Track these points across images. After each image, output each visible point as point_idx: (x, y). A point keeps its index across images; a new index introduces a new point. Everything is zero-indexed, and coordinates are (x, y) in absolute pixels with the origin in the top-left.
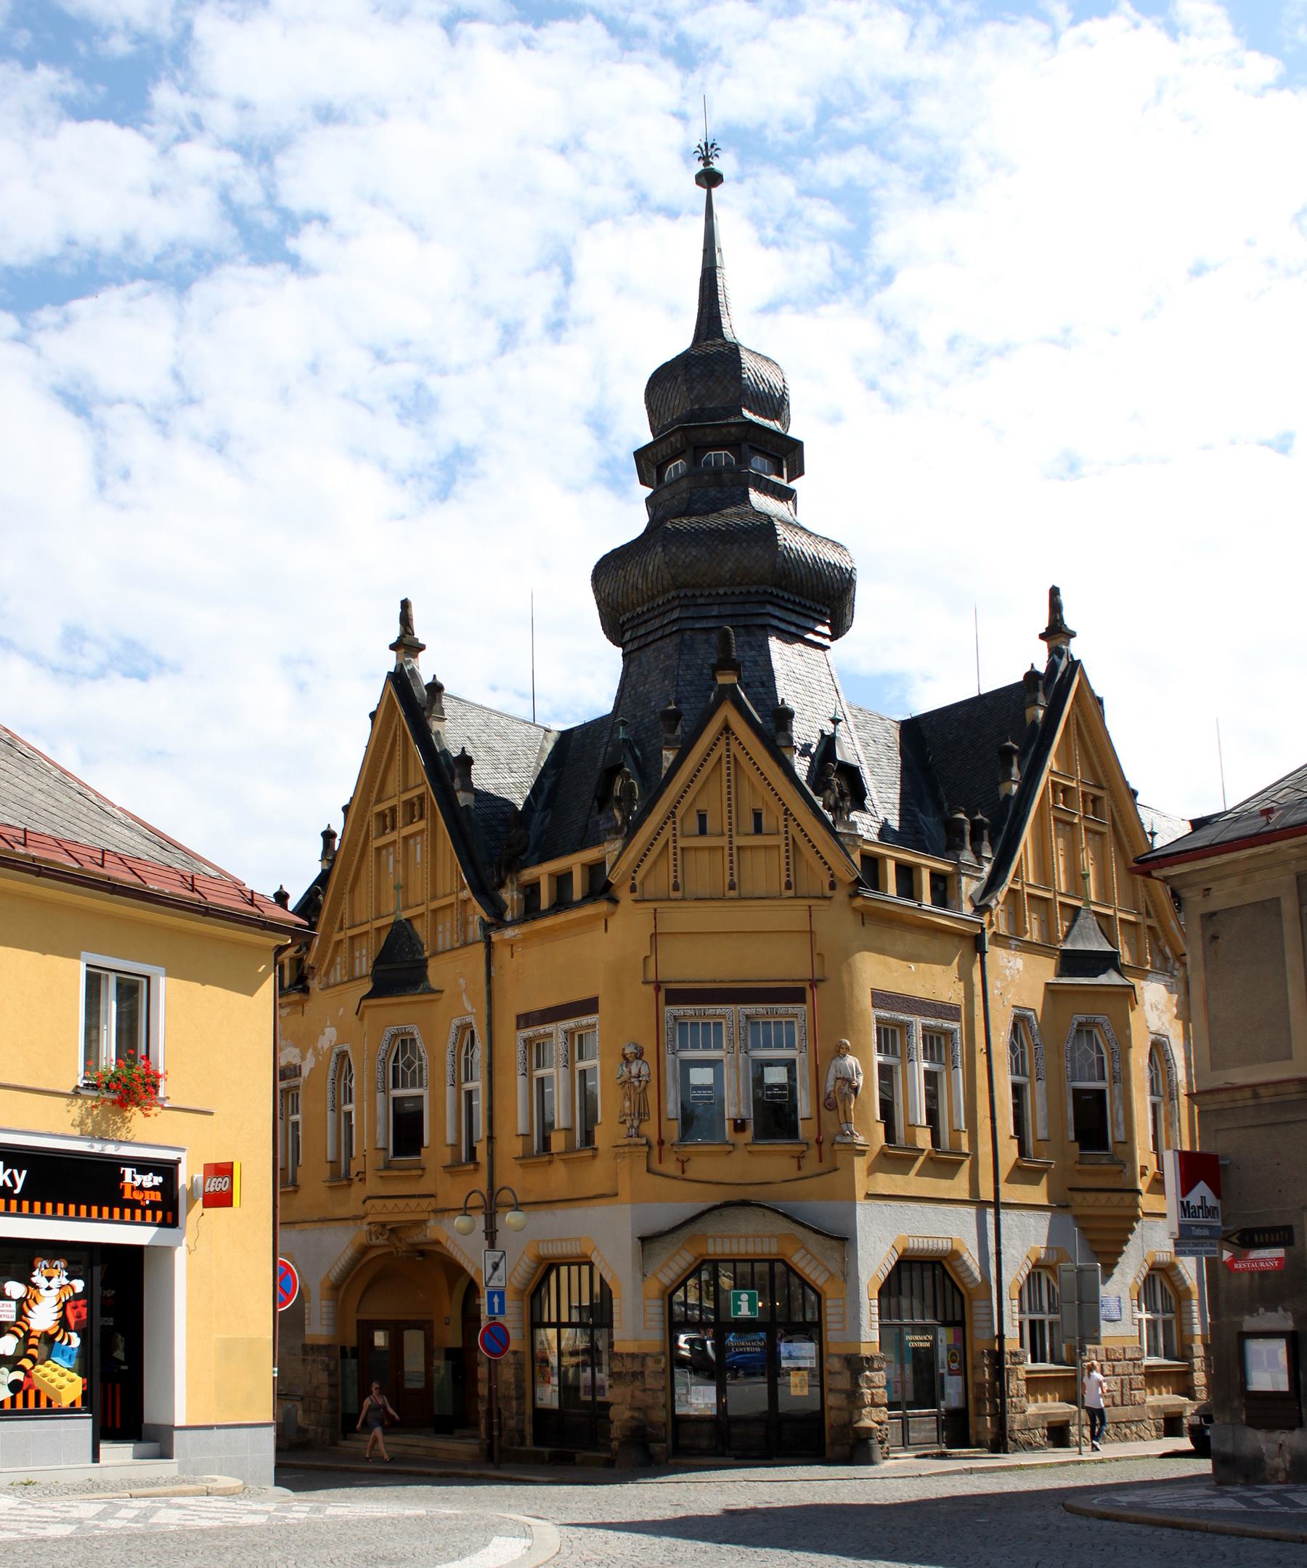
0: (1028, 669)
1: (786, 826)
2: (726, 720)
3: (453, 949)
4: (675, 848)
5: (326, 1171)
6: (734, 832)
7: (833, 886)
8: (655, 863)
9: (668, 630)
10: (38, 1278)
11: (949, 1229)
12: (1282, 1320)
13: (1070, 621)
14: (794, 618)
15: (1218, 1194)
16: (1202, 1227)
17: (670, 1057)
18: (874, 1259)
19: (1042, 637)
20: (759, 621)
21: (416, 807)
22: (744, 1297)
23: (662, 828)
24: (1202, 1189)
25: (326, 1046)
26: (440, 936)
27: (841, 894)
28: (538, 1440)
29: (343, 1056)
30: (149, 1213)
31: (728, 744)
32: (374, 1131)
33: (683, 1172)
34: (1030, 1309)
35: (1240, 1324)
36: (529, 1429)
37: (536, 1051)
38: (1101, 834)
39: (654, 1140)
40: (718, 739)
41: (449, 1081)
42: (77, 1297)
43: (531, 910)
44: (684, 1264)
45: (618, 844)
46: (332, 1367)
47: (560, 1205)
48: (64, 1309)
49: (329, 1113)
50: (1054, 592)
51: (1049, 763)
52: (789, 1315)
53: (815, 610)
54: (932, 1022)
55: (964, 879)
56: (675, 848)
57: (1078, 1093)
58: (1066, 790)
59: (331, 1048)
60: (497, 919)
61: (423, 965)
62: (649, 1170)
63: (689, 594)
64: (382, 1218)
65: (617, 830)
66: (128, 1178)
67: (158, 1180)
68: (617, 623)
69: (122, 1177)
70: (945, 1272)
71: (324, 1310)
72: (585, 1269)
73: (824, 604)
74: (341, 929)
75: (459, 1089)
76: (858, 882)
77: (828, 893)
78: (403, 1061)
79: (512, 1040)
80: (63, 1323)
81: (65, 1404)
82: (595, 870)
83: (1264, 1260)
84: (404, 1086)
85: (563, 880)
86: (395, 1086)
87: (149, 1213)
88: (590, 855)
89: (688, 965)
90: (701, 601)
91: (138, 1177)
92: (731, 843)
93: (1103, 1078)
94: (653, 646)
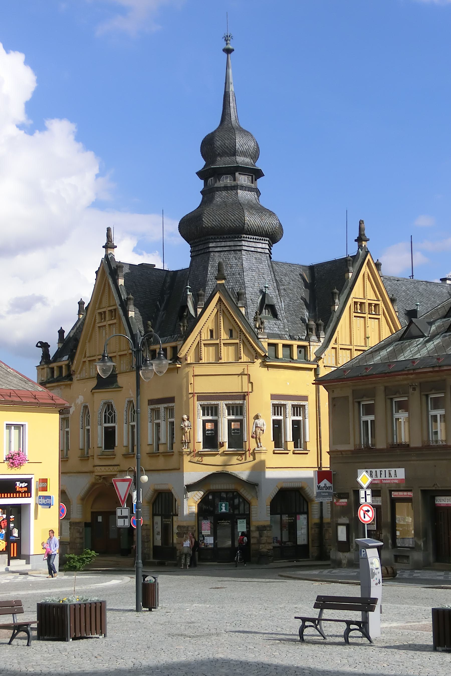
1: (240, 336)
5: (79, 453)
20: (238, 248)
21: (113, 313)
22: (224, 505)
25: (79, 403)
28: (154, 558)
29: (86, 407)
30: (23, 494)
32: (99, 439)
35: (337, 521)
36: (151, 553)
37: (156, 412)
41: (125, 421)
45: (182, 342)
46: (81, 531)
47: (161, 471)
52: (244, 512)
54: (296, 403)
59: (82, 404)
63: (213, 237)
64: (100, 474)
65: (182, 337)
66: (18, 485)
70: (301, 494)
74: (85, 357)
78: (109, 412)
79: (146, 410)
83: (343, 502)
84: (109, 422)
86: (105, 422)
87: (23, 494)
91: (21, 484)
92: (220, 342)
94: (201, 256)
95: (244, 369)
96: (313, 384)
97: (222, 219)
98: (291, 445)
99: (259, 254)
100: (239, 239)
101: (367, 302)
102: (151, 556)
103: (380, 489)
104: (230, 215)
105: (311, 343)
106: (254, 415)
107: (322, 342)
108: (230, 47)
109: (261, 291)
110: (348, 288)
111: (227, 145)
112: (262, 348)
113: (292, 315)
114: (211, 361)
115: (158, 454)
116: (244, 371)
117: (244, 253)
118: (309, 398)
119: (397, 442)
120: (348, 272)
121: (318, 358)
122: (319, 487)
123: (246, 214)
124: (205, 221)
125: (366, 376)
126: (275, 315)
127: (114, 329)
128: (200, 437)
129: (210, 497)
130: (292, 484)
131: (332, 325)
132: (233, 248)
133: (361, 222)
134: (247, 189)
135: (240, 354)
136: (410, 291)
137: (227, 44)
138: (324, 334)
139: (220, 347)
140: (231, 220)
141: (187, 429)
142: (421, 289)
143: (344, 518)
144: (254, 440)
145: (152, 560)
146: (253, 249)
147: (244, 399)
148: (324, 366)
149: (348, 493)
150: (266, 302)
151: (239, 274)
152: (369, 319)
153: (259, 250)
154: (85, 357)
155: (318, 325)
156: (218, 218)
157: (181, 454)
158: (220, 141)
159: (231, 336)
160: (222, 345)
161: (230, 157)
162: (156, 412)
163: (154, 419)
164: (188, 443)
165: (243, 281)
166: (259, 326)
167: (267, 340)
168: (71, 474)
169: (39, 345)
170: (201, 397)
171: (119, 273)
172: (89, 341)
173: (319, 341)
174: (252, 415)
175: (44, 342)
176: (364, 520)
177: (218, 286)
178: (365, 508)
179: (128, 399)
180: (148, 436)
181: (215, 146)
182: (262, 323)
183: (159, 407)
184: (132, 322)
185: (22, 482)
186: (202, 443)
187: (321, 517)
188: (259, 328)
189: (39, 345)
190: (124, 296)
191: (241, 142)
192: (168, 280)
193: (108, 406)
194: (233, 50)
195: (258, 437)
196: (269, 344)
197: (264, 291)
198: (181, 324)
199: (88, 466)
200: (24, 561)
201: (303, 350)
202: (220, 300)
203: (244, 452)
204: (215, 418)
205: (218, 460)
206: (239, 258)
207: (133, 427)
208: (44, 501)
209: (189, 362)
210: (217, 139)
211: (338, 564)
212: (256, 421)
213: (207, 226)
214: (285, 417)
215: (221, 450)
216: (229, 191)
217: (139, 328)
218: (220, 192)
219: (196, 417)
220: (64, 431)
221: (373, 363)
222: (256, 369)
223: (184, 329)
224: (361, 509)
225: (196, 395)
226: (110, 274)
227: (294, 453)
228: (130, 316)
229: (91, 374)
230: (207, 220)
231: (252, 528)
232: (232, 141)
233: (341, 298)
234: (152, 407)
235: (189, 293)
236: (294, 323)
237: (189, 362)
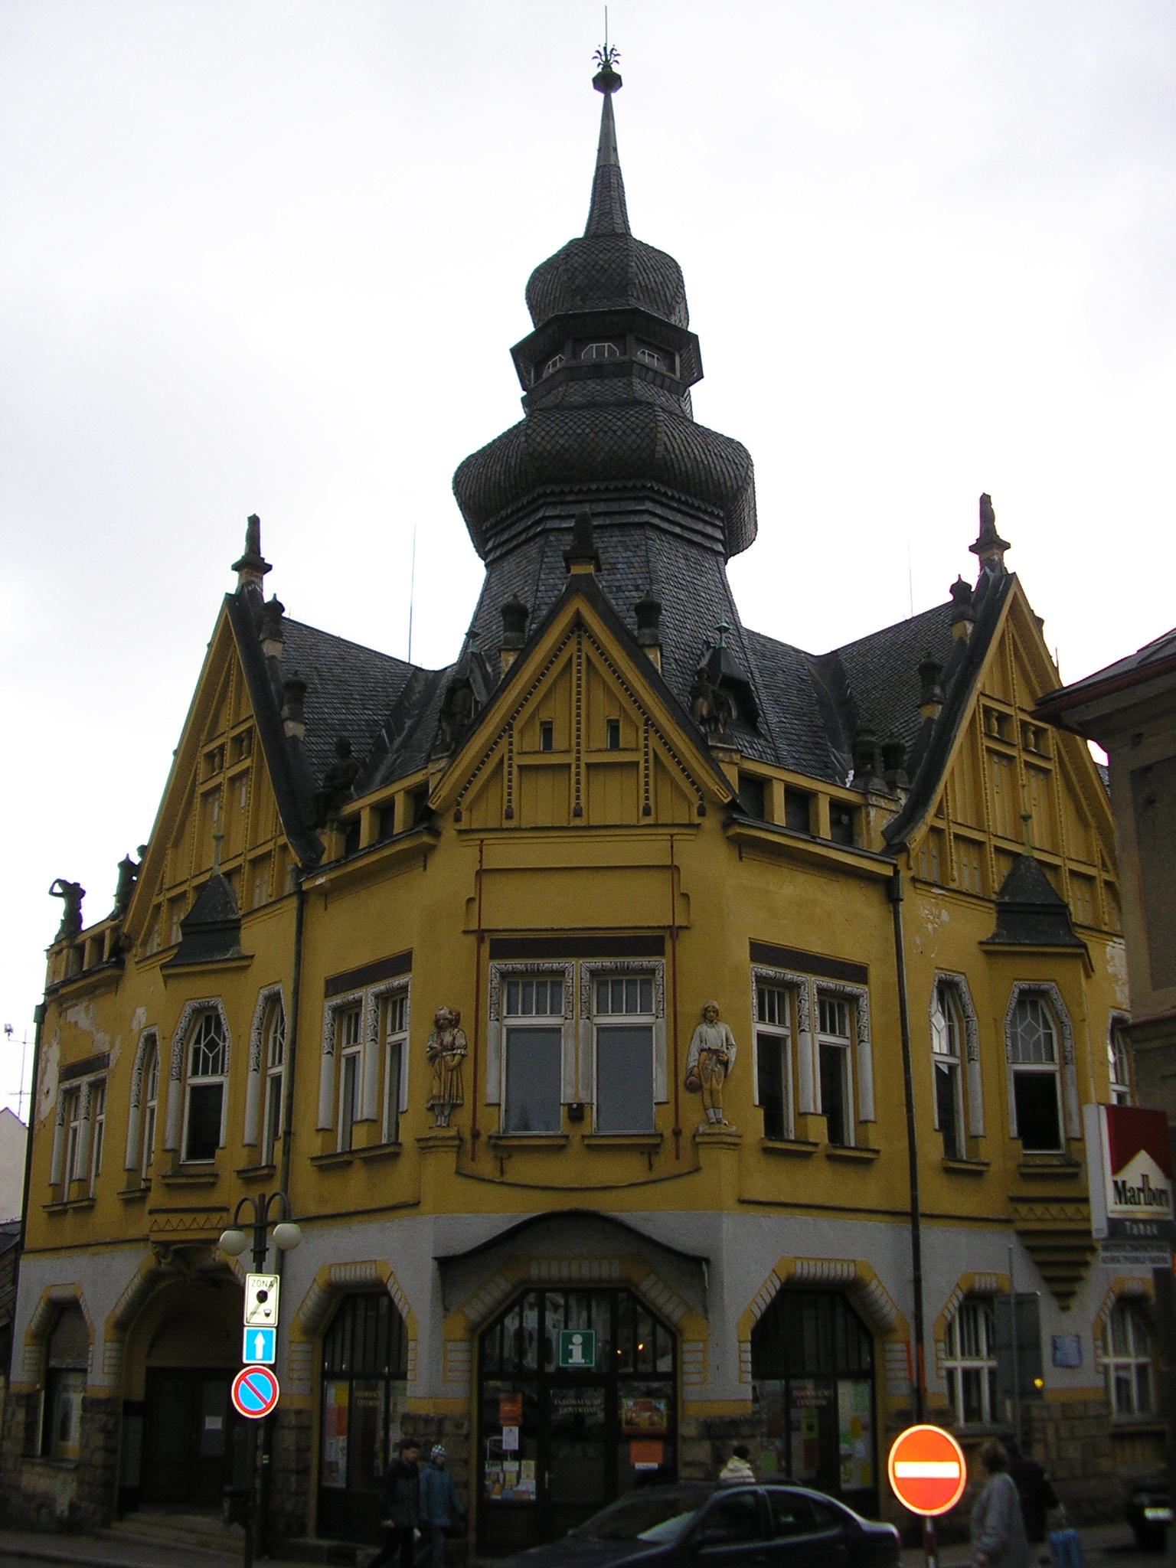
0: (955, 580)
1: (646, 739)
2: (578, 613)
4: (510, 766)
6: (583, 748)
7: (702, 812)
8: (485, 787)
9: (531, 533)
11: (854, 1247)
13: (1003, 531)
14: (679, 518)
17: (492, 1025)
18: (745, 1286)
19: (972, 549)
23: (496, 743)
27: (711, 822)
31: (579, 643)
33: (502, 1173)
37: (347, 1015)
38: (1046, 772)
39: (467, 1135)
40: (568, 638)
41: (252, 1064)
44: (498, 1294)
47: (355, 1219)
49: (132, 1110)
50: (985, 501)
51: (979, 686)
53: (705, 512)
54: (830, 983)
55: (873, 812)
56: (510, 766)
57: (1021, 1079)
58: (1003, 718)
60: (310, 867)
61: (235, 926)
62: (459, 1173)
71: (878, 1293)
73: (715, 505)
76: (733, 806)
77: (697, 820)
80: (1003, 1404)
82: (418, 795)
84: (205, 1072)
85: (384, 811)
89: (520, 909)
90: (571, 498)
92: (578, 759)
93: (1052, 1059)
102: (311, 1524)
107: (903, 802)
118: (873, 974)
130: (839, 1266)
132: (617, 520)
138: (906, 778)
145: (311, 1540)
146: (678, 530)
168: (96, 1249)
169: (58, 889)
179: (265, 992)
180: (319, 1105)
183: (357, 996)
192: (419, 687)
193: (208, 1019)
199: (143, 1224)
202: (578, 624)
207: (277, 1080)
220: (95, 1120)
222: (707, 858)
234: (337, 1000)
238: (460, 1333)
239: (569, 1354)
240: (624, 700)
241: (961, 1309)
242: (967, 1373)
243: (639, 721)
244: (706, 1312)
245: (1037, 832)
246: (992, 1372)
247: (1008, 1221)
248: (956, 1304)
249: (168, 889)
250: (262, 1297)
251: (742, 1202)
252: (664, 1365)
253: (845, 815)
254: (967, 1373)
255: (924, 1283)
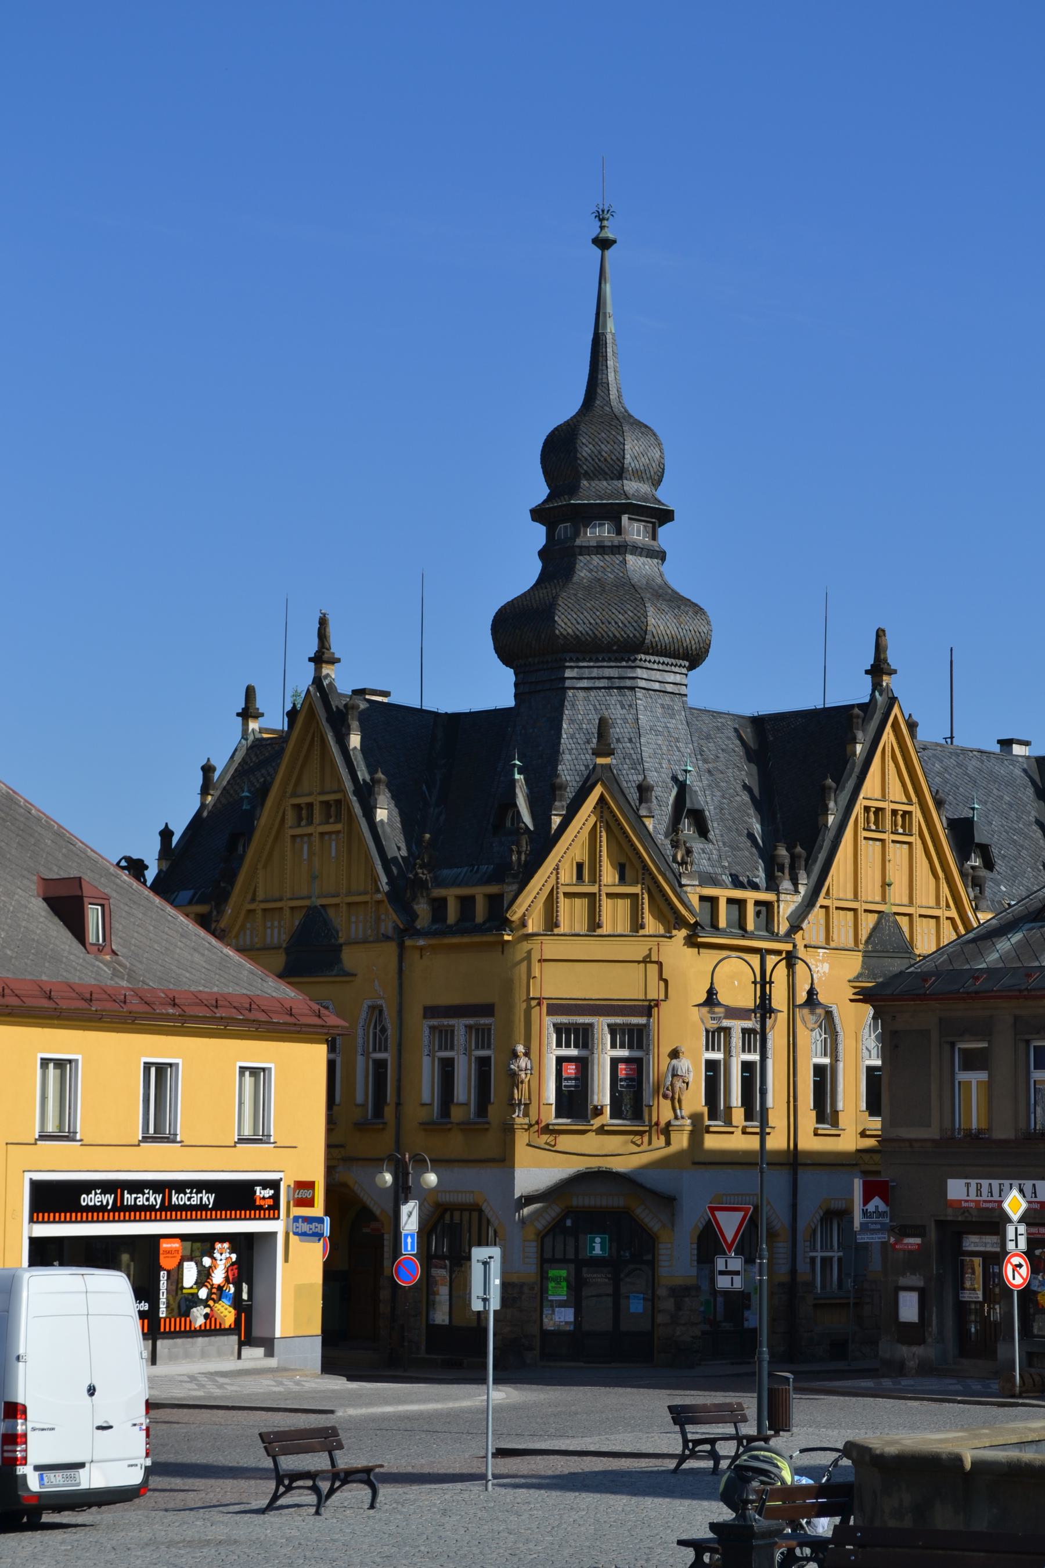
3: (365, 941)
10: (217, 1255)
12: (917, 1281)
14: (658, 676)
15: (887, 1203)
16: (875, 1223)
20: (628, 683)
22: (598, 1240)
24: (876, 1202)
26: (353, 926)
34: (822, 1248)
37: (445, 1037)
41: (360, 1050)
42: (233, 1264)
43: (439, 926)
45: (515, 887)
48: (227, 1272)
61: (339, 948)
66: (258, 1193)
67: (272, 1192)
68: (506, 654)
69: (255, 1192)
72: (475, 1215)
74: (253, 900)
75: (368, 1058)
80: (227, 1280)
81: (227, 1326)
83: (911, 1244)
85: (467, 903)
88: (493, 889)
92: (600, 890)
95: (650, 950)
96: (852, 1001)
97: (598, 621)
98: (738, 1115)
99: (667, 697)
100: (630, 664)
101: (888, 806)
102: (423, 1347)
103: (997, 1220)
104: (614, 611)
105: (782, 897)
106: (669, 1050)
108: (609, 234)
109: (675, 779)
110: (854, 776)
111: (603, 453)
112: (688, 904)
113: (730, 829)
114: (577, 930)
115: (449, 1126)
116: (649, 955)
117: (640, 694)
119: (1035, 1128)
120: (854, 741)
121: (795, 927)
122: (865, 1213)
123: (651, 610)
124: (560, 622)
125: (976, 993)
126: (703, 832)
127: (333, 844)
128: (550, 1094)
129: (569, 1223)
131: (822, 857)
133: (880, 634)
134: (644, 553)
135: (643, 918)
136: (950, 774)
137: (602, 228)
138: (805, 876)
139: (600, 900)
140: (616, 623)
141: (523, 1076)
142: (970, 770)
143: (914, 1277)
144: (669, 1102)
146: (657, 686)
147: (649, 1015)
148: (806, 946)
149: (924, 1227)
150: (688, 805)
151: (630, 740)
152: (891, 845)
153: (669, 688)
154: (253, 900)
155: (794, 858)
156: (589, 617)
157: (509, 1130)
158: (591, 446)
159: (622, 880)
160: (604, 897)
161: (610, 482)
162: (445, 1037)
163: (437, 1048)
164: (525, 1104)
165: (639, 756)
166: (683, 858)
167: (698, 889)
169: (123, 863)
170: (554, 1009)
171: (350, 721)
172: (265, 867)
173: (797, 891)
174: (666, 1050)
175: (135, 857)
176: (1014, 1282)
177: (599, 770)
178: (1016, 1260)
179: (369, 1002)
181: (579, 456)
182: (689, 852)
184: (384, 831)
185: (264, 1188)
186: (554, 1106)
187: (793, 1272)
188: (683, 863)
189: (123, 863)
190: (363, 774)
191: (633, 449)
194: (614, 242)
195: (677, 1096)
196: (702, 898)
197: (681, 778)
198: (514, 847)
200: (260, 1351)
201: (763, 909)
202: (602, 799)
203: (647, 1128)
204: (584, 1053)
205: (591, 1143)
206: (630, 706)
208: (305, 1227)
209: (530, 929)
210: (584, 441)
211: (898, 1369)
212: (674, 1062)
213: (565, 633)
214: (728, 1053)
215: (597, 1122)
216: (606, 557)
217: (397, 845)
218: (588, 557)
219: (544, 1048)
221: (984, 966)
222: (675, 950)
223: (519, 859)
224: (1009, 1261)
225: (545, 1002)
226: (328, 720)
227: (744, 1133)
228: (378, 819)
229: (268, 940)
230: (566, 620)
231: (662, 1292)
232: (616, 446)
233: (839, 799)
234: (434, 1022)
235: (517, 776)
236: (734, 848)
237: (530, 931)
238: (532, 1237)
239: (593, 1248)
240: (631, 854)
241: (822, 1220)
242: (824, 1260)
243: (639, 866)
244: (673, 1226)
245: (898, 894)
246: (840, 1259)
247: (856, 1165)
248: (818, 1218)
249: (262, 902)
250: (410, 1215)
251: (695, 1163)
252: (649, 1257)
253: (766, 909)
254: (824, 1260)
255: (799, 1207)
